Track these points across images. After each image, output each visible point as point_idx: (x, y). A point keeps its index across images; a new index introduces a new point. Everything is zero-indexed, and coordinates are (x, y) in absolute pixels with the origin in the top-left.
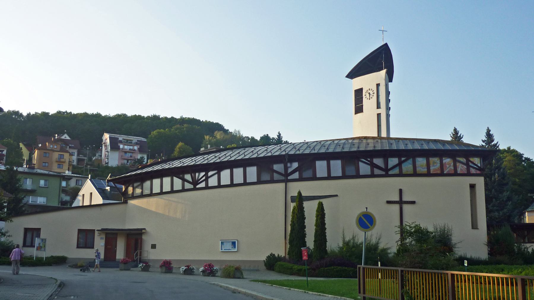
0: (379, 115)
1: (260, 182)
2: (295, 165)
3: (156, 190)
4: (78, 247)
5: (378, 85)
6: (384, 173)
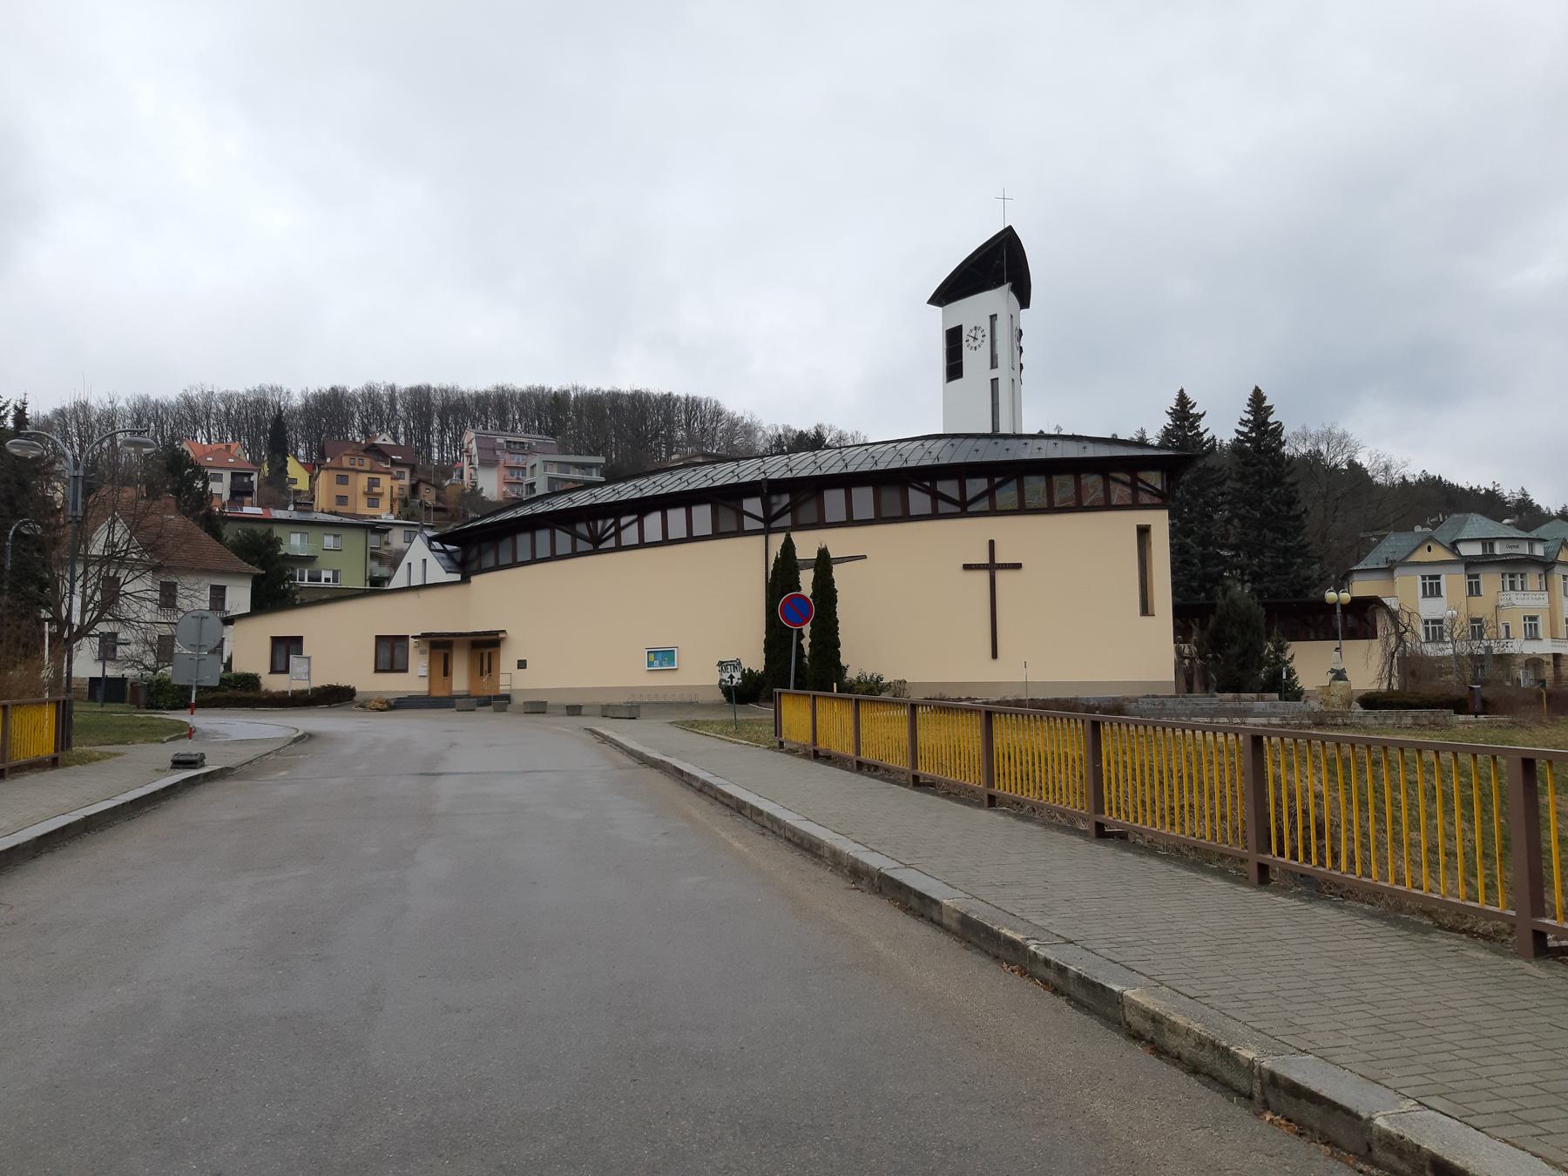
0: (994, 381)
1: (717, 534)
2: (786, 499)
4: (377, 671)
5: (993, 318)
6: (958, 509)
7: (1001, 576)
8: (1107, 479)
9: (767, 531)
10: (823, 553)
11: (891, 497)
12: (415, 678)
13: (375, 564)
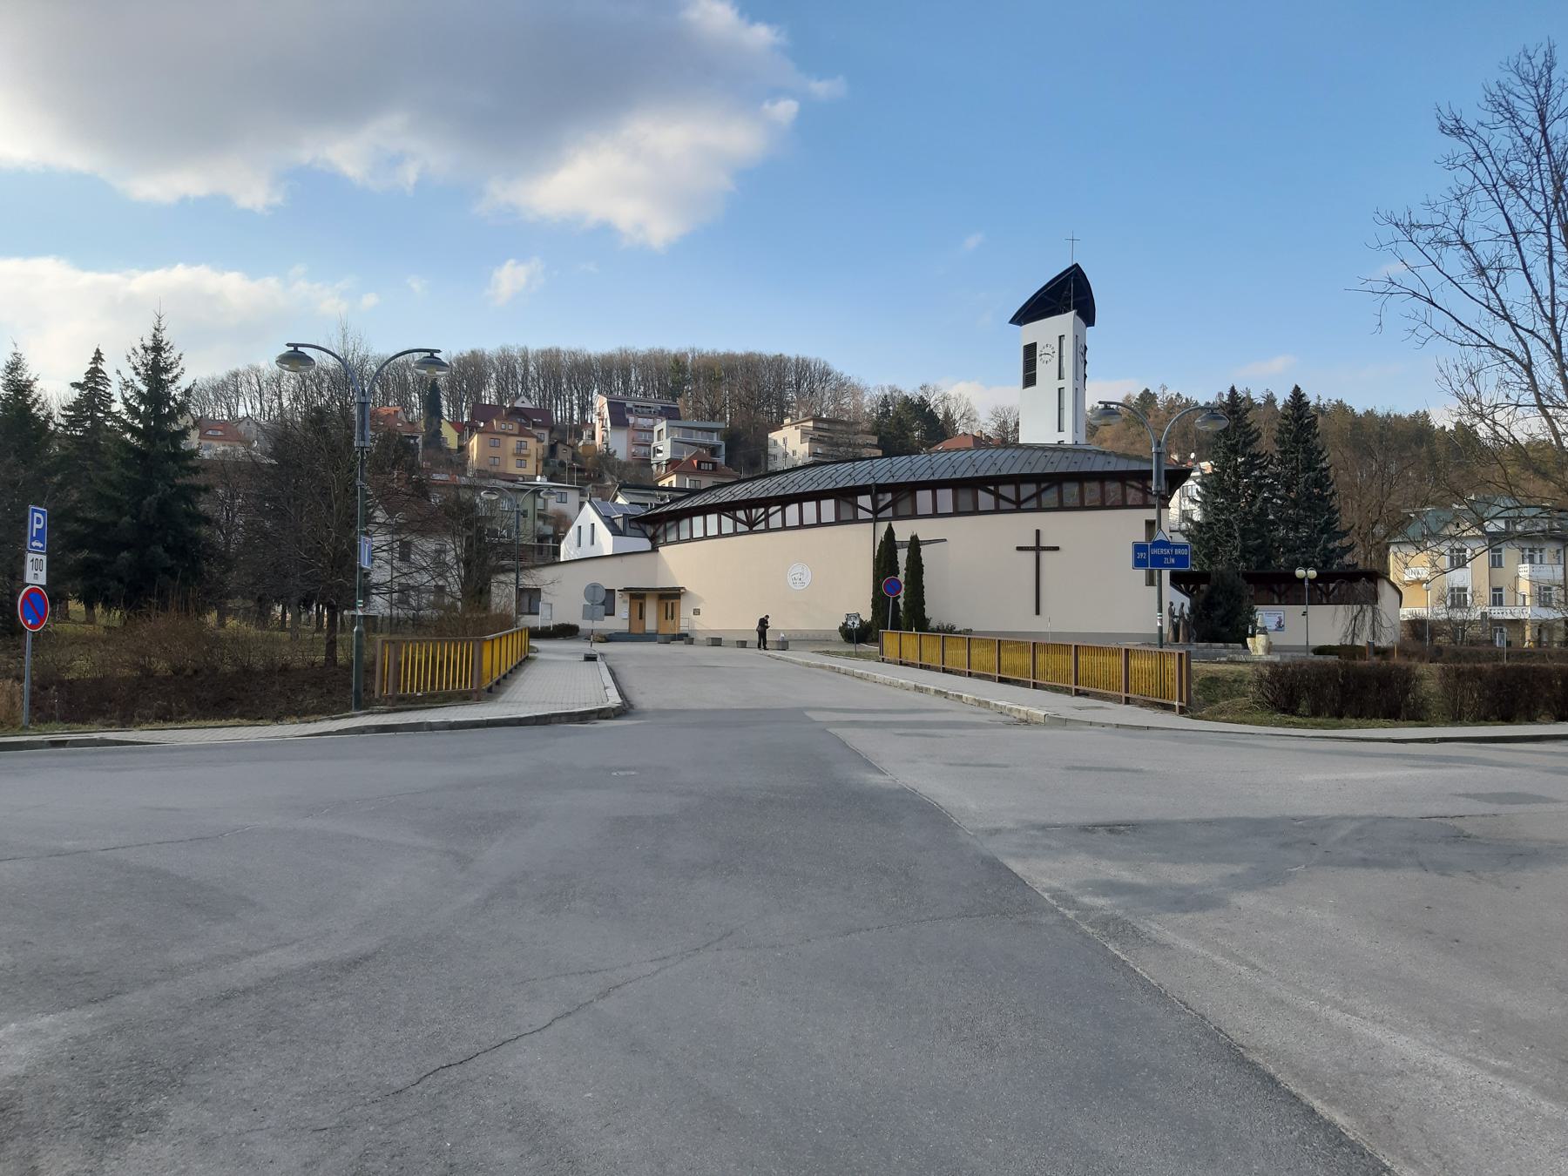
1: (839, 521)
2: (889, 497)
3: (698, 533)
7: (1044, 554)
8: (1124, 484)
9: (876, 520)
10: (914, 539)
11: (965, 497)
12: (620, 620)
13: (540, 523)
